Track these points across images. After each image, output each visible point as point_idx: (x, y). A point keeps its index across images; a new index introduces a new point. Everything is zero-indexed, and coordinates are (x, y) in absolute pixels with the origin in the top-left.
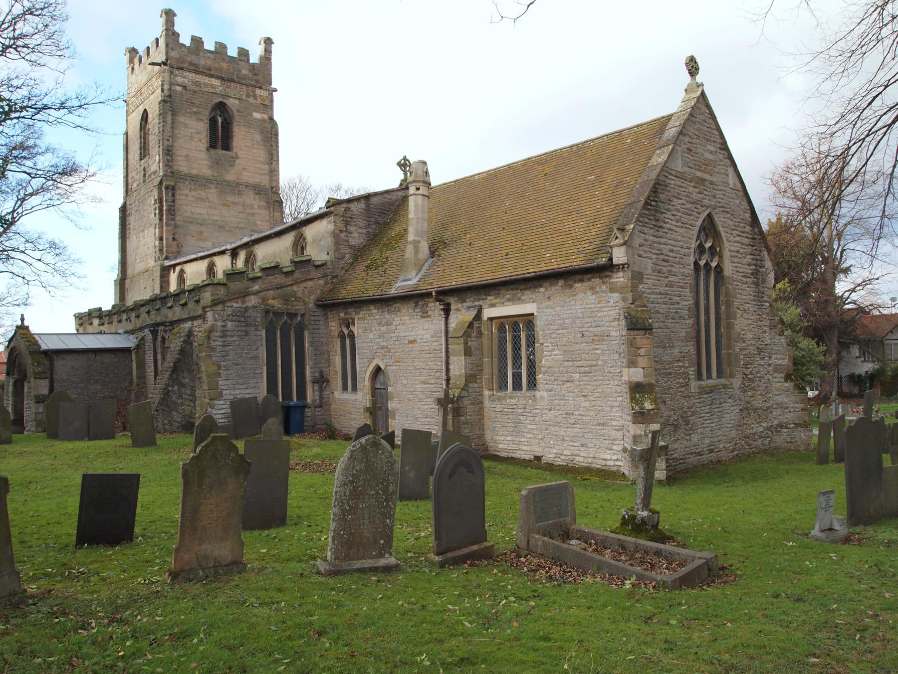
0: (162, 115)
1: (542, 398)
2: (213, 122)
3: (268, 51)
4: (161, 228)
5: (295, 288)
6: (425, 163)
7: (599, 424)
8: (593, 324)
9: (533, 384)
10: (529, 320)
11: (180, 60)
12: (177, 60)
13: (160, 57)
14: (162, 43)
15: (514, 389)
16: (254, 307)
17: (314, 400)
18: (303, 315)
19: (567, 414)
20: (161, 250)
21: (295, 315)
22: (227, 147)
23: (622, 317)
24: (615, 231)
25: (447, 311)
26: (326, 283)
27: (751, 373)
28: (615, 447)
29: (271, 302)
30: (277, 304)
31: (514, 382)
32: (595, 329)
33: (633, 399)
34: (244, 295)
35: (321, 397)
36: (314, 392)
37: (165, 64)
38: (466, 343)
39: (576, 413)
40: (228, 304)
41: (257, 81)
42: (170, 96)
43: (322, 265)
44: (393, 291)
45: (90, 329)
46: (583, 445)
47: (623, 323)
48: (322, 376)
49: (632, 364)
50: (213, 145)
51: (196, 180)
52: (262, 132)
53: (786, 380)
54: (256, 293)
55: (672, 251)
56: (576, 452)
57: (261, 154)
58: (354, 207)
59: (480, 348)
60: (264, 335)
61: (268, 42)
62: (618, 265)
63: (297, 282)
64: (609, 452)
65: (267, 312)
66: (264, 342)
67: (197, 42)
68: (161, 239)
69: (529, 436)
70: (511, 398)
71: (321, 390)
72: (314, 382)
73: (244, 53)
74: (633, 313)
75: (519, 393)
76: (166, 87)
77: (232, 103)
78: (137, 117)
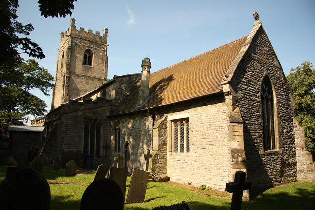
0: (68, 53)
1: (192, 156)
2: (85, 56)
3: (106, 33)
4: (64, 91)
5: (98, 110)
6: (148, 59)
7: (217, 169)
8: (215, 121)
9: (188, 150)
10: (187, 119)
11: (76, 35)
12: (75, 35)
13: (69, 34)
14: (70, 29)
15: (180, 152)
16: (80, 116)
17: (103, 155)
18: (101, 120)
19: (203, 163)
20: (63, 99)
21: (97, 120)
22: (90, 64)
23: (228, 117)
24: (224, 77)
25: (154, 119)
26: (111, 108)
27: (287, 147)
28: (224, 180)
29: (87, 114)
30: (90, 115)
31: (180, 149)
32: (216, 123)
33: (233, 157)
34: (76, 111)
35: (106, 155)
36: (103, 151)
37: (70, 36)
38: (159, 131)
39: (207, 163)
40: (70, 114)
41: (102, 42)
42: (71, 46)
43: (109, 101)
44: (133, 110)
45: (34, 125)
46: (210, 179)
47: (229, 120)
48: (107, 145)
49: (233, 139)
50: (84, 63)
51: (79, 76)
52: (103, 60)
53: (302, 150)
54: (82, 110)
55: (251, 89)
56: (206, 182)
57: (102, 67)
58: (124, 79)
59: (166, 134)
60: (83, 127)
61: (107, 30)
62: (226, 93)
63: (99, 107)
64: (222, 182)
65: (85, 118)
66: (83, 130)
67: (82, 29)
68: (63, 95)
69: (186, 173)
70: (179, 156)
71: (106, 151)
72: (103, 148)
73: (98, 33)
74: (233, 115)
75: (182, 154)
76: (70, 43)
77: (93, 50)
78: (61, 54)
